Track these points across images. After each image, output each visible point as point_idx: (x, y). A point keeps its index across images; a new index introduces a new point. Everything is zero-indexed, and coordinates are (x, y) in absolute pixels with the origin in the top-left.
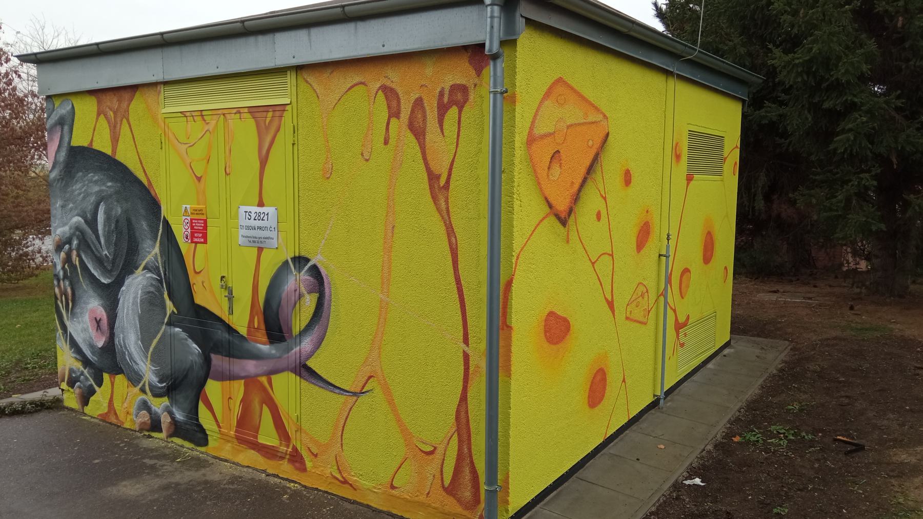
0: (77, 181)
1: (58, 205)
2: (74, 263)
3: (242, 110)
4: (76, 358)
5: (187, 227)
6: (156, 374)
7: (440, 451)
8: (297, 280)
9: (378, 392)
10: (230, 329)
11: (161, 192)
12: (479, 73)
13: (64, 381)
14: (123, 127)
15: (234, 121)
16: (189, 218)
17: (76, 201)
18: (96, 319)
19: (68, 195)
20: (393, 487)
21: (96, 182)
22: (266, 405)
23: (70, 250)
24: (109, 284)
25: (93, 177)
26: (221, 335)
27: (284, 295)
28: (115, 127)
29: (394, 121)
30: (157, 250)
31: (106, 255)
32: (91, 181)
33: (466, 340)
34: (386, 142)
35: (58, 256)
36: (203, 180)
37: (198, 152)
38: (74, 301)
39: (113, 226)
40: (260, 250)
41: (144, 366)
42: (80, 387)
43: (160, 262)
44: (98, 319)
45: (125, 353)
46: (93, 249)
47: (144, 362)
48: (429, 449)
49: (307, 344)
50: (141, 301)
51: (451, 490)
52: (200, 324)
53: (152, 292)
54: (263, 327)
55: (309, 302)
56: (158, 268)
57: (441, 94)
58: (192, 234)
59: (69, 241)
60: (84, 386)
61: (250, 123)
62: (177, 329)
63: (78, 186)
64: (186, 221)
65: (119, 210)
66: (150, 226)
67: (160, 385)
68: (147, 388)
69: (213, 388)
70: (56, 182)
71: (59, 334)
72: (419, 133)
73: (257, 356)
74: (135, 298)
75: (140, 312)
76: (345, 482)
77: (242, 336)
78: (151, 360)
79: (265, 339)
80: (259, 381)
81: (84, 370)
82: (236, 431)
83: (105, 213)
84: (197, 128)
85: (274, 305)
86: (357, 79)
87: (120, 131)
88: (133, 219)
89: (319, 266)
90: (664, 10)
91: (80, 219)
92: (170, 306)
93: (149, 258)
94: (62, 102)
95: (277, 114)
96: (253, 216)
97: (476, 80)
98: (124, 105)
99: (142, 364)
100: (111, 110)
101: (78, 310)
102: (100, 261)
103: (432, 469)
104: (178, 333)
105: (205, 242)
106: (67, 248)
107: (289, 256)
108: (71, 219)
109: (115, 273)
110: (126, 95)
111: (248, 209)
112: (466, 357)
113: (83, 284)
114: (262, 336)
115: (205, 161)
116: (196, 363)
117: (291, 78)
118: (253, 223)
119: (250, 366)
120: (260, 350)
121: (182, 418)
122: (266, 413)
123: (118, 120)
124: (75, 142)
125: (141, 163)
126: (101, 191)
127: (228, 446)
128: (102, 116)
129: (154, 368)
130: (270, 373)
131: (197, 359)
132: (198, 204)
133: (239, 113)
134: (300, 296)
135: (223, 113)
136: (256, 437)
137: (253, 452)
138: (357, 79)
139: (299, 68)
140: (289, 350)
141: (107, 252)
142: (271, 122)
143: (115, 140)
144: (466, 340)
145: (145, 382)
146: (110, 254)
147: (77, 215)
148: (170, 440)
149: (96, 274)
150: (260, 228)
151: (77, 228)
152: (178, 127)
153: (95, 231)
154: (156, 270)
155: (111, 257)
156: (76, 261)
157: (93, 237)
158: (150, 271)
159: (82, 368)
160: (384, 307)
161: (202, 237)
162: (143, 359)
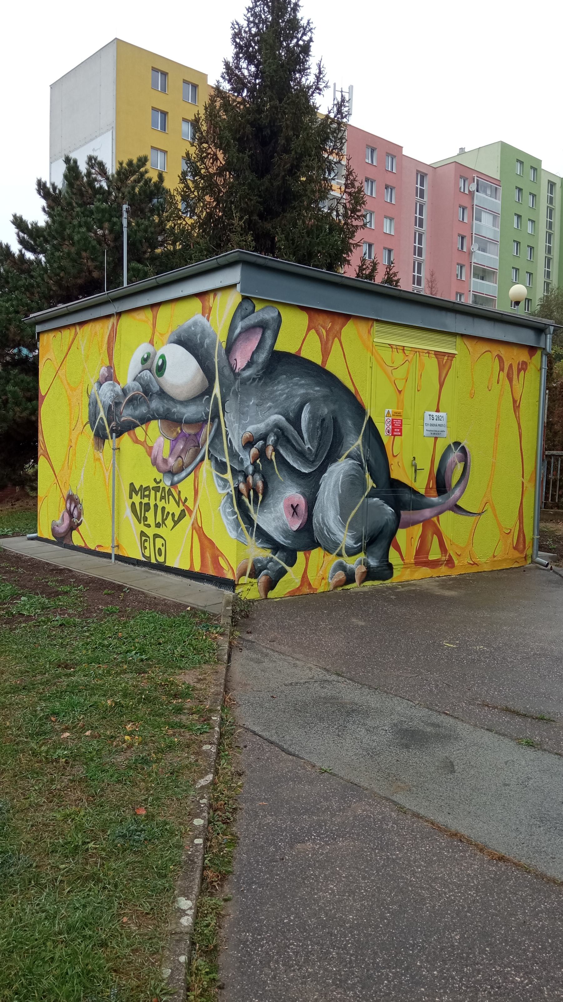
0: (279, 383)
1: (251, 403)
2: (269, 458)
3: (430, 352)
4: (263, 548)
5: (388, 425)
6: (353, 538)
7: (512, 531)
8: (455, 455)
9: (490, 510)
10: (415, 492)
11: (365, 398)
12: (531, 358)
13: (245, 575)
14: (334, 345)
15: (425, 357)
16: (391, 418)
17: (277, 400)
18: (292, 506)
19: (266, 394)
20: (494, 556)
21: (302, 386)
22: (436, 535)
23: (265, 446)
24: (310, 474)
25: (300, 381)
26: (407, 496)
27: (448, 465)
28: (327, 343)
29: (501, 372)
30: (359, 442)
31: (309, 448)
32: (296, 384)
33: (523, 477)
34: (498, 383)
35: (247, 453)
36: (402, 393)
37: (399, 374)
38: (265, 494)
39: (318, 423)
40: (436, 438)
41: (342, 535)
42: (266, 575)
43: (361, 451)
44: (295, 505)
45: (323, 529)
46: (294, 444)
47: (341, 531)
48: (508, 531)
49: (457, 492)
50: (342, 483)
51: (515, 548)
52: (394, 492)
53: (353, 475)
54: (435, 487)
55: (460, 468)
56: (360, 456)
57: (519, 364)
58: (393, 430)
59: (264, 437)
60: (273, 571)
61: (434, 361)
62: (375, 499)
63: (281, 387)
64: (388, 420)
65: (326, 411)
66: (354, 424)
67: (355, 546)
68: (344, 552)
69: (401, 535)
70: (251, 381)
71: (242, 529)
72: (510, 380)
73: (431, 506)
74: (336, 481)
75: (340, 492)
76: (475, 564)
77: (422, 495)
78: (348, 529)
79: (435, 494)
80: (432, 521)
81: (273, 556)
82: (415, 559)
83: (310, 412)
84: (399, 357)
85: (443, 472)
86: (488, 349)
87: (331, 347)
88: (339, 419)
89: (466, 446)
90: (16, 255)
91: (280, 417)
92: (370, 483)
93: (353, 448)
94: (266, 307)
95: (450, 358)
96: (435, 418)
97: (530, 361)
98: (337, 327)
99: (340, 533)
100: (324, 328)
101: (270, 501)
102: (301, 454)
103: (510, 541)
104: (375, 502)
105: (401, 435)
106: (261, 444)
107: (451, 441)
108: (269, 416)
109: (318, 464)
110: (340, 321)
111: (432, 413)
112: (523, 483)
113: (279, 476)
114: (434, 492)
115: (404, 381)
116: (390, 520)
117: (459, 340)
118: (434, 422)
119: (427, 513)
120: (432, 501)
121: (376, 564)
122: (435, 538)
123: (331, 338)
124: (278, 347)
125: (350, 375)
126: (307, 394)
127: (408, 571)
128: (313, 332)
129: (350, 534)
130: (437, 515)
131: (391, 517)
132: (397, 409)
133: (429, 353)
134: (456, 464)
135: (415, 351)
136: (427, 557)
137: (424, 568)
138: (488, 349)
139: (462, 335)
140: (449, 497)
141: (310, 446)
142: (446, 362)
143: (326, 353)
144: (523, 477)
145: (342, 548)
146: (313, 447)
147: (276, 413)
148: (362, 585)
149: (295, 466)
150: (439, 425)
151: (277, 425)
152: (386, 354)
153: (298, 428)
154: (358, 458)
155: (314, 450)
156: (271, 456)
157: (295, 433)
158: (353, 459)
159: (271, 555)
160: (494, 465)
161: (399, 432)
162: (341, 529)
